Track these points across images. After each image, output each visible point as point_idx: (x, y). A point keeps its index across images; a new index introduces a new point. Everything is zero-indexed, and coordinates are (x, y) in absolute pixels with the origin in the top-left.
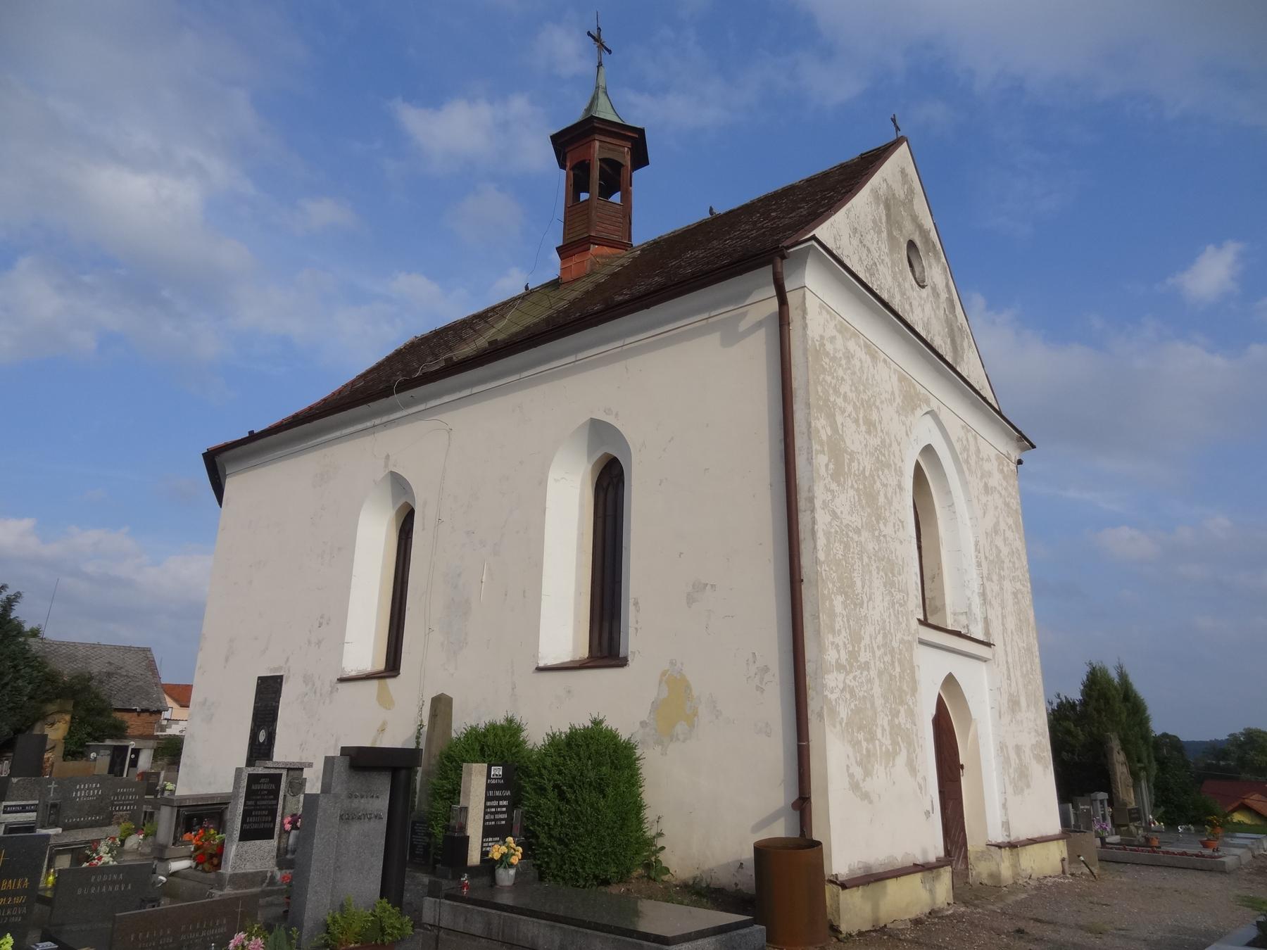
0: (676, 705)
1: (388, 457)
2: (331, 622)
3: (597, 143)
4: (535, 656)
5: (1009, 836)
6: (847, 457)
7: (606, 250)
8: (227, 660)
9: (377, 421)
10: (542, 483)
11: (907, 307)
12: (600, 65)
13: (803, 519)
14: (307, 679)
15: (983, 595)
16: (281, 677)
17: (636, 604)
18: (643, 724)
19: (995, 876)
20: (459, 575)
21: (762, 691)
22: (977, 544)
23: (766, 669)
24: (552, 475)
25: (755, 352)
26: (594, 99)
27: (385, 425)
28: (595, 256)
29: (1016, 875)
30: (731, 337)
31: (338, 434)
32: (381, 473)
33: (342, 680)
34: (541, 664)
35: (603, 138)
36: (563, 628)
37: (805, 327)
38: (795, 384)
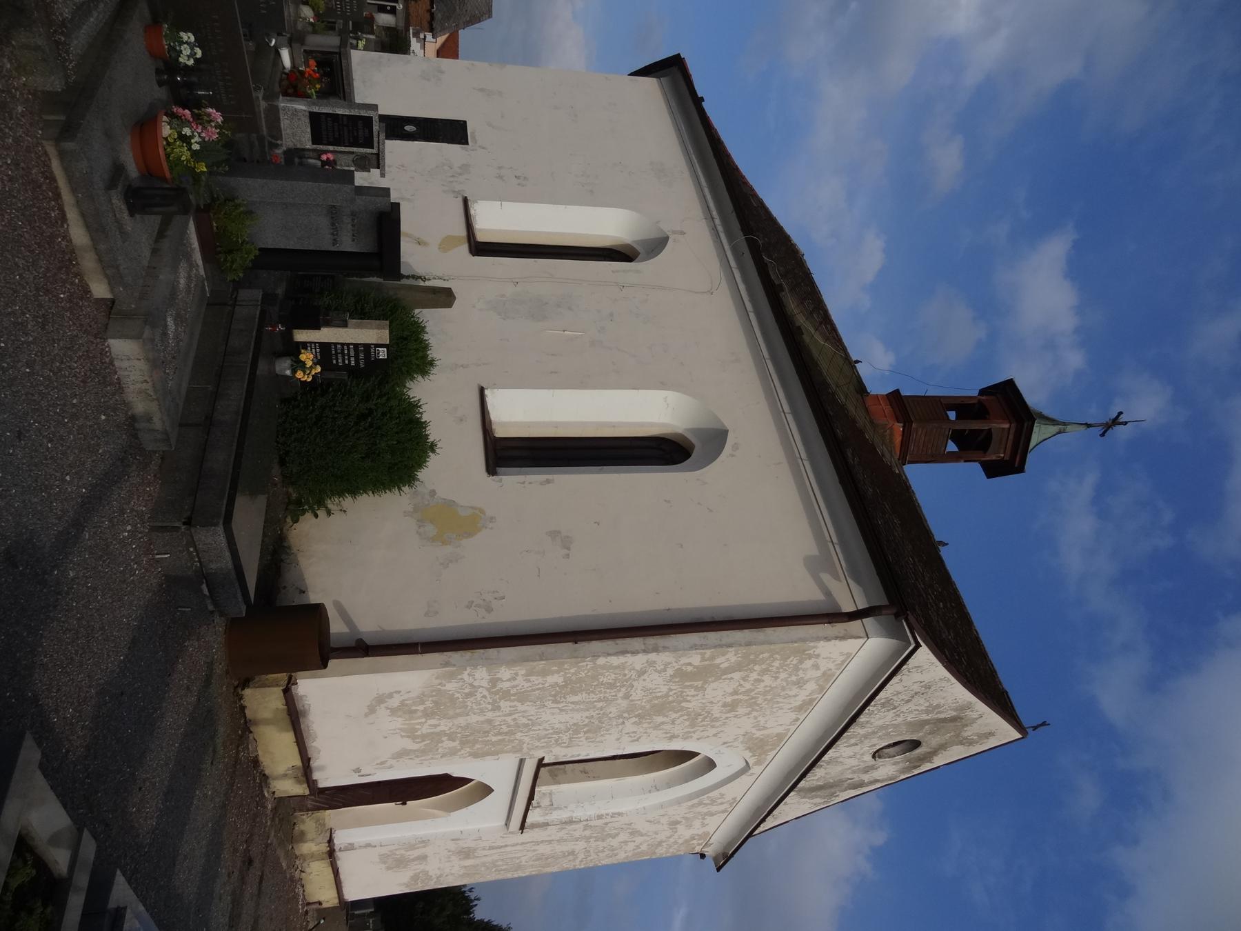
0: (453, 524)
1: (682, 233)
2: (521, 187)
3: (1007, 426)
4: (495, 386)
5: (340, 850)
6: (700, 684)
7: (898, 439)
8: (482, 90)
9: (718, 221)
10: (663, 385)
11: (853, 741)
12: (1089, 426)
13: (636, 643)
14: (465, 168)
15: (570, 822)
16: (467, 143)
17: (548, 482)
18: (433, 493)
19: (302, 837)
20: (570, 309)
21: (469, 607)
22: (620, 814)
23: (489, 610)
24: (671, 395)
25: (800, 590)
26: (1053, 422)
27: (714, 229)
28: (891, 428)
29: (304, 858)
30: (815, 566)
31: (704, 183)
32: (666, 228)
33: (465, 201)
34: (487, 392)
35: (1012, 431)
36: (522, 411)
37: (827, 639)
38: (769, 631)
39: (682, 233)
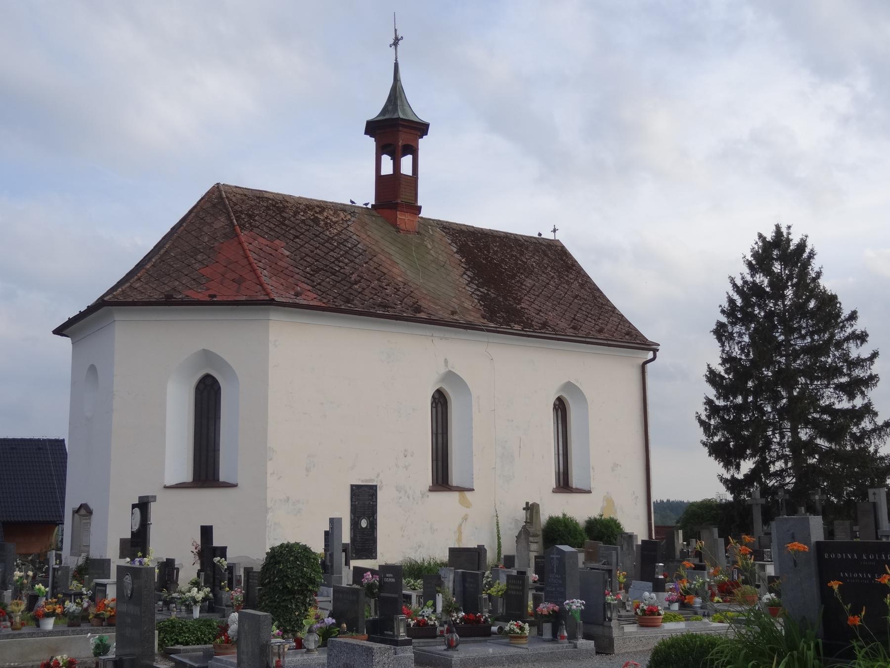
1: (446, 361)
8: (308, 470)
32: (443, 370)
34: (169, 483)
39: (446, 361)
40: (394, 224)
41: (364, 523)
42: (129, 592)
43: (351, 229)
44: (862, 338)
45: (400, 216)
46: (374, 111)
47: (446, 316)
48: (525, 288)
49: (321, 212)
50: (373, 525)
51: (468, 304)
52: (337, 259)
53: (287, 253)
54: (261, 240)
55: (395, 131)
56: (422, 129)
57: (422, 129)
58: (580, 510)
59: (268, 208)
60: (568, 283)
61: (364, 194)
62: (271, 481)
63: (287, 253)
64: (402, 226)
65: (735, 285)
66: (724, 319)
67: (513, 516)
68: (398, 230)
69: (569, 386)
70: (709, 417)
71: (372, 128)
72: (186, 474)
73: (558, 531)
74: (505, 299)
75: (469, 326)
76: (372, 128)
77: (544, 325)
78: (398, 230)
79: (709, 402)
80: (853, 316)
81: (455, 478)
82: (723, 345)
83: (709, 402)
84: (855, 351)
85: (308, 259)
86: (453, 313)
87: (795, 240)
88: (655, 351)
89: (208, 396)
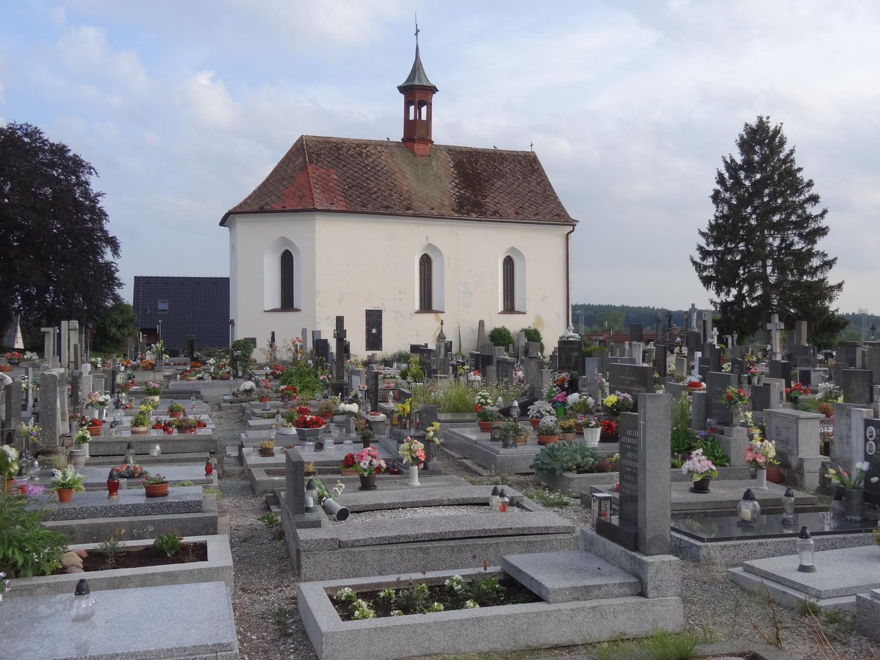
0: (539, 319)
8: (340, 302)
25: (560, 242)
32: (425, 243)
40: (413, 152)
41: (374, 331)
42: (495, 425)
43: (383, 157)
44: (814, 199)
45: (416, 146)
46: (402, 80)
47: (427, 211)
48: (499, 186)
49: (365, 148)
50: (380, 332)
51: (446, 203)
52: (368, 179)
53: (336, 177)
54: (321, 170)
55: (417, 92)
56: (433, 90)
57: (433, 90)
58: (514, 324)
59: (331, 149)
60: (529, 182)
61: (397, 134)
62: (318, 308)
63: (336, 177)
64: (418, 152)
65: (726, 162)
66: (719, 187)
67: (469, 326)
68: (415, 155)
69: (513, 249)
70: (703, 259)
71: (402, 89)
72: (278, 305)
73: (500, 337)
74: (476, 196)
75: (441, 217)
76: (402, 89)
77: (495, 213)
78: (415, 155)
79: (700, 248)
80: (810, 184)
81: (435, 307)
82: (718, 207)
83: (700, 248)
84: (812, 210)
85: (348, 180)
86: (432, 209)
87: (772, 126)
88: (574, 226)
89: (287, 261)
